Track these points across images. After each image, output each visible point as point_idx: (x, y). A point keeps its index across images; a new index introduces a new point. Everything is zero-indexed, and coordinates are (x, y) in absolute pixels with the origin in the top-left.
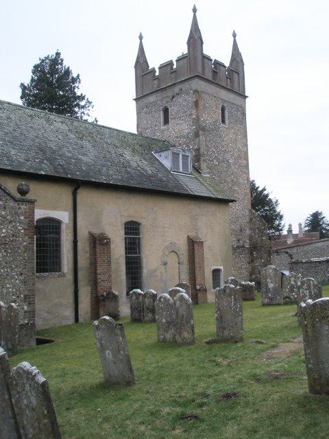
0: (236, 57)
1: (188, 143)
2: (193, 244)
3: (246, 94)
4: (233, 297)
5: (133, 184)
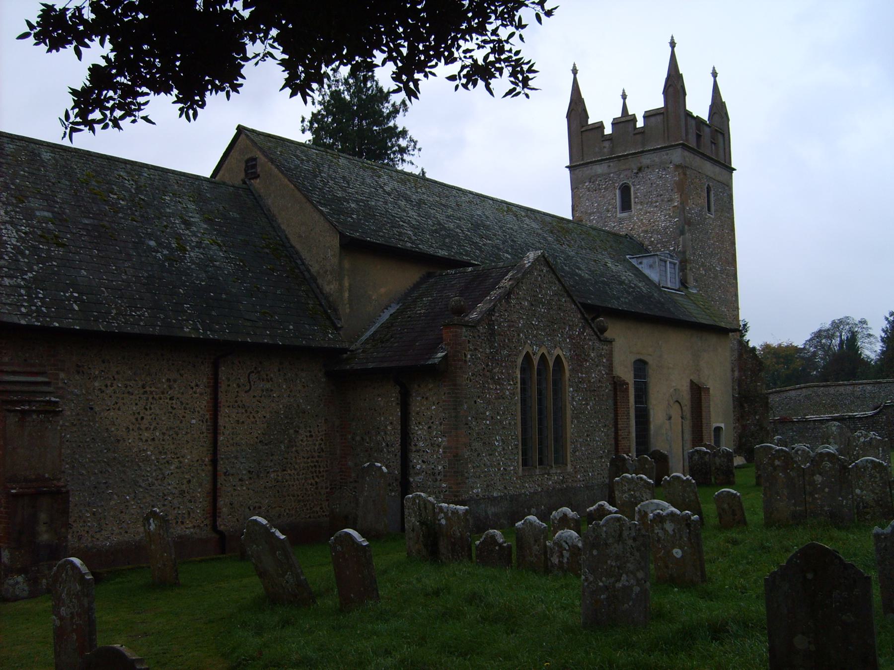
0: (718, 107)
1: (667, 242)
2: (698, 392)
3: (733, 166)
4: (880, 449)
5: (641, 308)
